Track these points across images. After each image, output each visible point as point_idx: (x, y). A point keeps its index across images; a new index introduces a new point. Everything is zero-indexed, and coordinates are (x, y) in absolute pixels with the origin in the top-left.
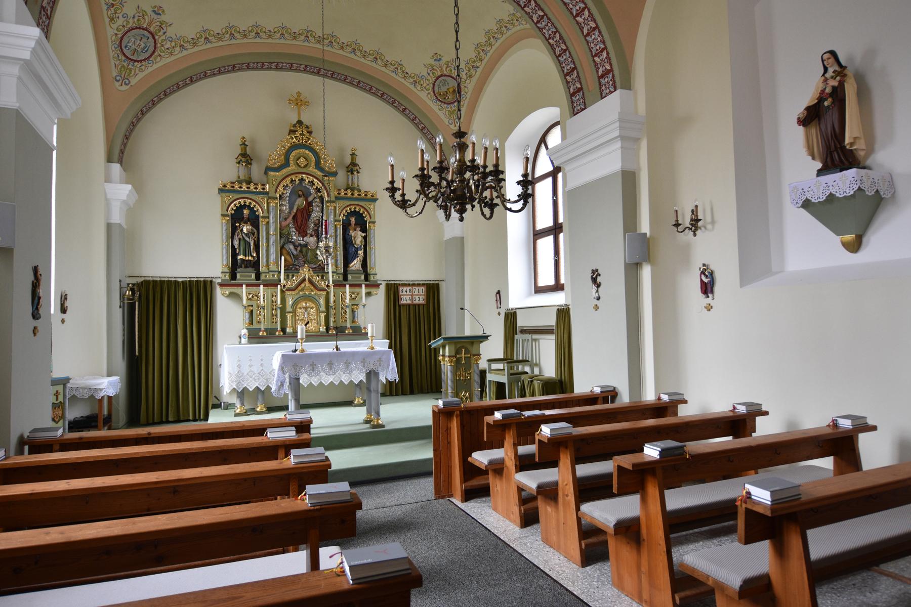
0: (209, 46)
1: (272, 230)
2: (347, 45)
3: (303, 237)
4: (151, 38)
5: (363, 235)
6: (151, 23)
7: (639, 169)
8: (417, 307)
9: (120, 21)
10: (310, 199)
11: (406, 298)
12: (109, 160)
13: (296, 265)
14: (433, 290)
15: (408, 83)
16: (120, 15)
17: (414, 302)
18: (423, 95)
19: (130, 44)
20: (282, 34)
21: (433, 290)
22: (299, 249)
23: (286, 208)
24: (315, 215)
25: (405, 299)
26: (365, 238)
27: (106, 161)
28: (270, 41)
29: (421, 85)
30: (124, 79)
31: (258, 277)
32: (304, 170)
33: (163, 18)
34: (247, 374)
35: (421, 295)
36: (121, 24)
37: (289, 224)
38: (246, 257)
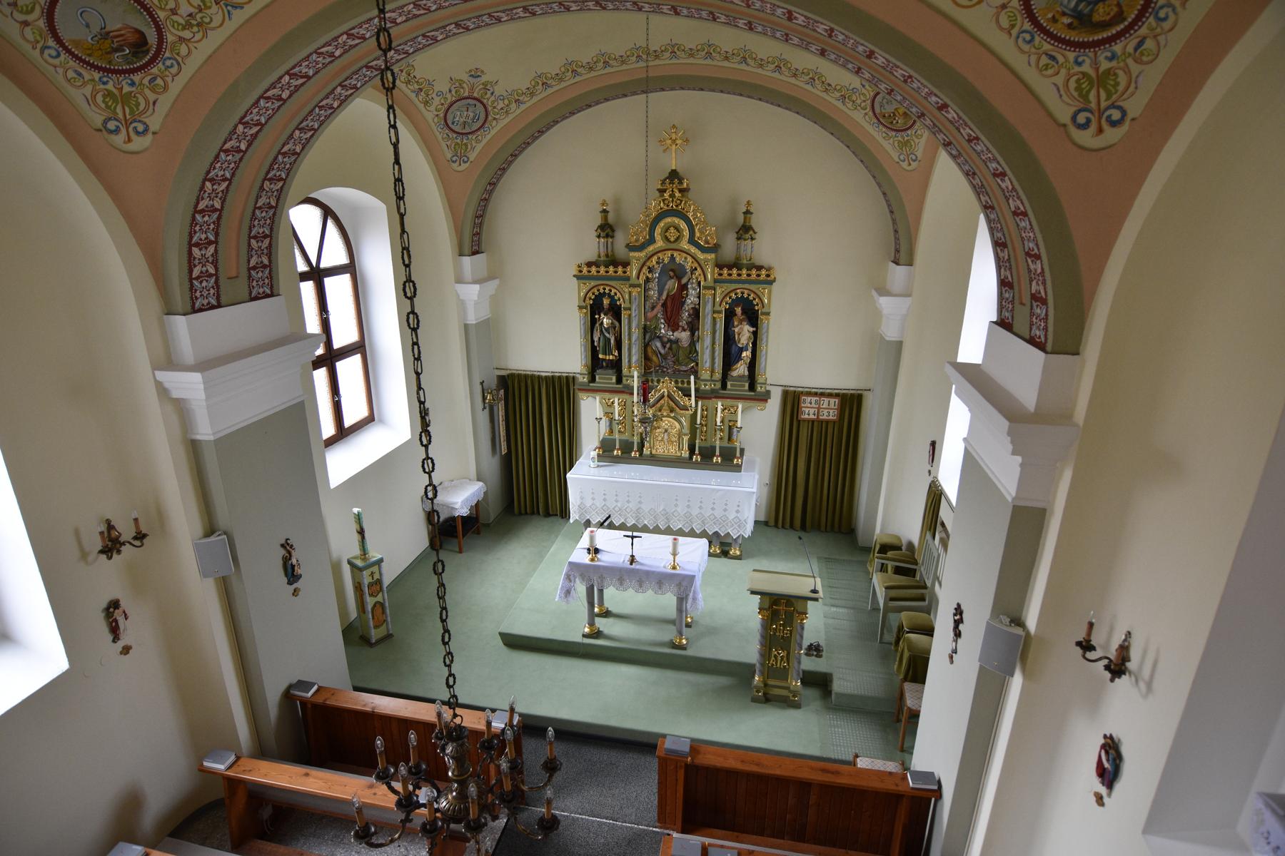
0: (550, 91)
2: (733, 54)
3: (673, 331)
4: (478, 104)
6: (472, 89)
9: (437, 101)
10: (684, 281)
11: (809, 410)
13: (663, 366)
14: (851, 403)
15: (832, 98)
16: (434, 95)
17: (821, 417)
18: (858, 116)
19: (457, 119)
20: (639, 56)
21: (851, 403)
22: (668, 346)
23: (653, 293)
24: (691, 300)
25: (807, 412)
26: (755, 334)
28: (624, 67)
29: (854, 102)
30: (461, 157)
33: (484, 79)
34: (590, 506)
35: (831, 409)
36: (433, 116)
37: (657, 315)
38: (606, 355)
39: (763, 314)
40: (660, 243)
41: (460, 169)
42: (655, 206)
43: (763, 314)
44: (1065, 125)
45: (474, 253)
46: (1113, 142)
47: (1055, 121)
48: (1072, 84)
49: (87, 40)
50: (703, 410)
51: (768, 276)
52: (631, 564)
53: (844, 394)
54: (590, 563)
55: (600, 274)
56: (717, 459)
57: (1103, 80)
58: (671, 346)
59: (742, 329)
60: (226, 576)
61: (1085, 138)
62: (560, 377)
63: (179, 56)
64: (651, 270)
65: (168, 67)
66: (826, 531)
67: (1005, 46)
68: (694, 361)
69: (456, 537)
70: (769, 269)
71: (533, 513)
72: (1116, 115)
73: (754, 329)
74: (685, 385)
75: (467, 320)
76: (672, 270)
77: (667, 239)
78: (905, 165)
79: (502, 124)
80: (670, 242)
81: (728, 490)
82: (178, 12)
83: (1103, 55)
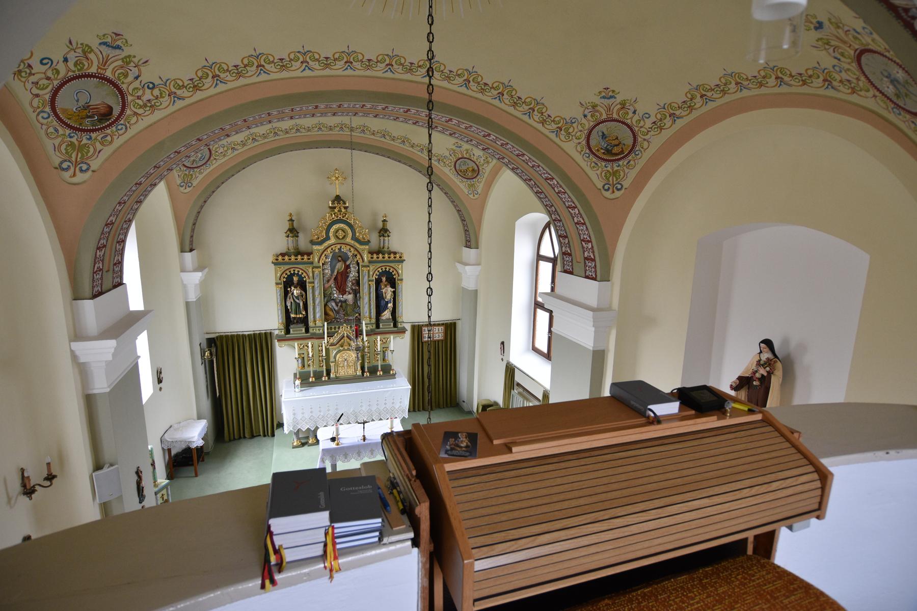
0: (256, 143)
1: (317, 293)
3: (343, 295)
5: (393, 290)
7: (608, 350)
8: (437, 342)
10: (348, 263)
12: (182, 251)
13: (337, 318)
14: (450, 328)
18: (446, 170)
21: (450, 328)
22: (339, 304)
23: (328, 272)
24: (353, 274)
26: (394, 292)
27: (180, 251)
30: (187, 182)
31: (307, 331)
32: (342, 241)
34: (301, 419)
37: (331, 286)
38: (297, 314)
39: (398, 280)
40: (333, 240)
41: (186, 191)
42: (329, 218)
43: (398, 280)
44: (600, 189)
45: (191, 250)
46: (618, 196)
47: (596, 187)
48: (603, 174)
49: (73, 110)
50: (322, 351)
51: (400, 257)
52: (364, 441)
53: (446, 323)
54: (337, 446)
55: (385, 259)
56: (367, 374)
57: (615, 173)
58: (342, 304)
59: (387, 290)
60: (109, 502)
61: (608, 194)
62: (260, 334)
63: (128, 123)
64: (326, 257)
65: (118, 130)
66: (444, 408)
67: (578, 158)
68: (357, 313)
69: (192, 465)
70: (401, 253)
71: (240, 438)
72: (619, 187)
73: (394, 290)
74: (333, 330)
75: (188, 299)
76: (340, 256)
77: (337, 237)
78: (471, 196)
79: (219, 162)
80: (339, 239)
81: (394, 390)
82: (142, 98)
83: (615, 165)
